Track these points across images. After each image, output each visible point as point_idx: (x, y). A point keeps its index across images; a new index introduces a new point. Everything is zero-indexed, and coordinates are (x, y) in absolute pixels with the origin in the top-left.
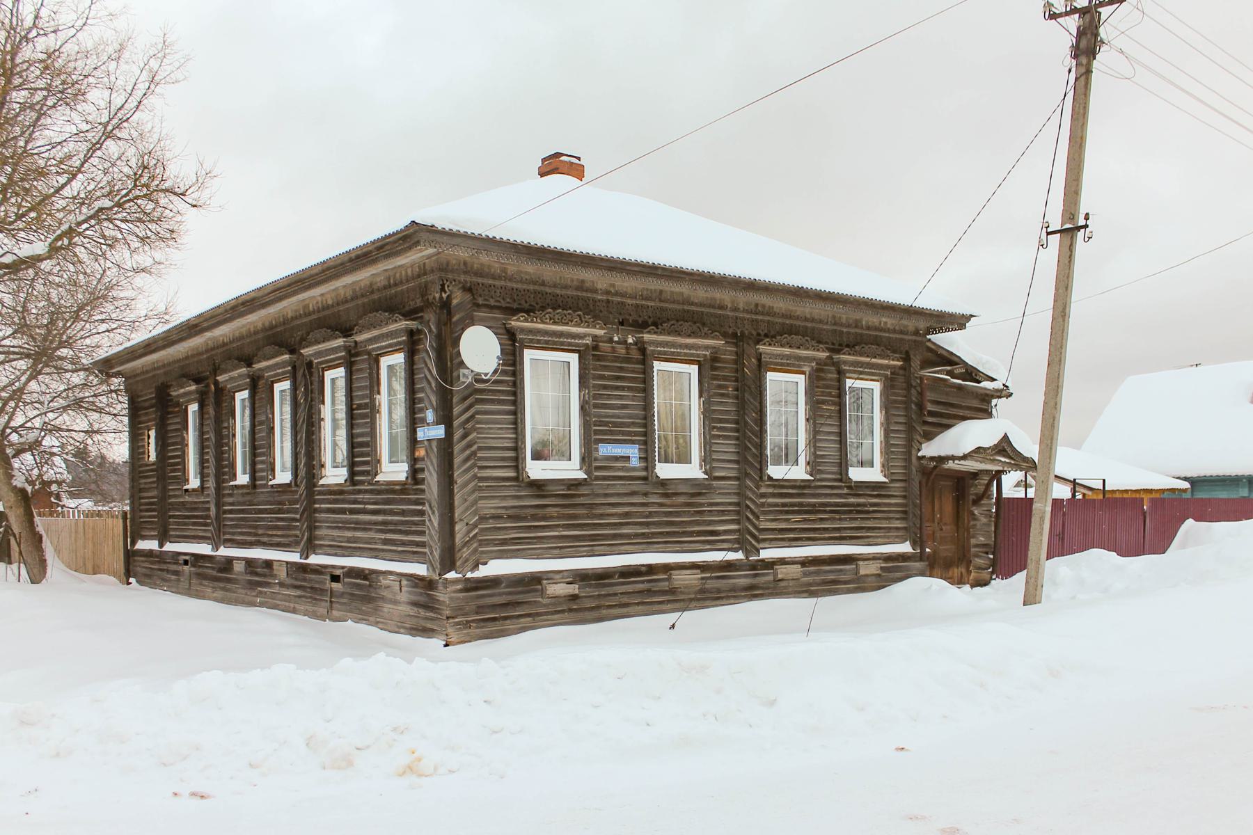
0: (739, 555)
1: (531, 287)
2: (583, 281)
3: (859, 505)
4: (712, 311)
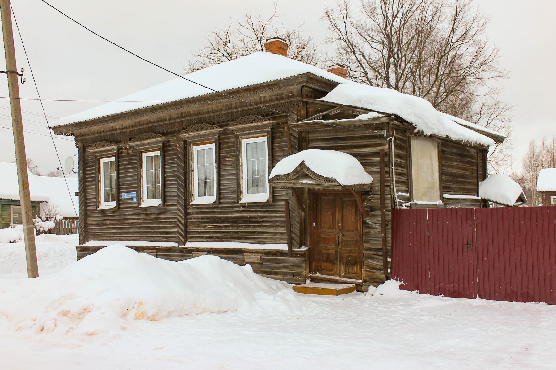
0: (175, 245)
2: (112, 127)
3: (250, 218)
4: (159, 124)
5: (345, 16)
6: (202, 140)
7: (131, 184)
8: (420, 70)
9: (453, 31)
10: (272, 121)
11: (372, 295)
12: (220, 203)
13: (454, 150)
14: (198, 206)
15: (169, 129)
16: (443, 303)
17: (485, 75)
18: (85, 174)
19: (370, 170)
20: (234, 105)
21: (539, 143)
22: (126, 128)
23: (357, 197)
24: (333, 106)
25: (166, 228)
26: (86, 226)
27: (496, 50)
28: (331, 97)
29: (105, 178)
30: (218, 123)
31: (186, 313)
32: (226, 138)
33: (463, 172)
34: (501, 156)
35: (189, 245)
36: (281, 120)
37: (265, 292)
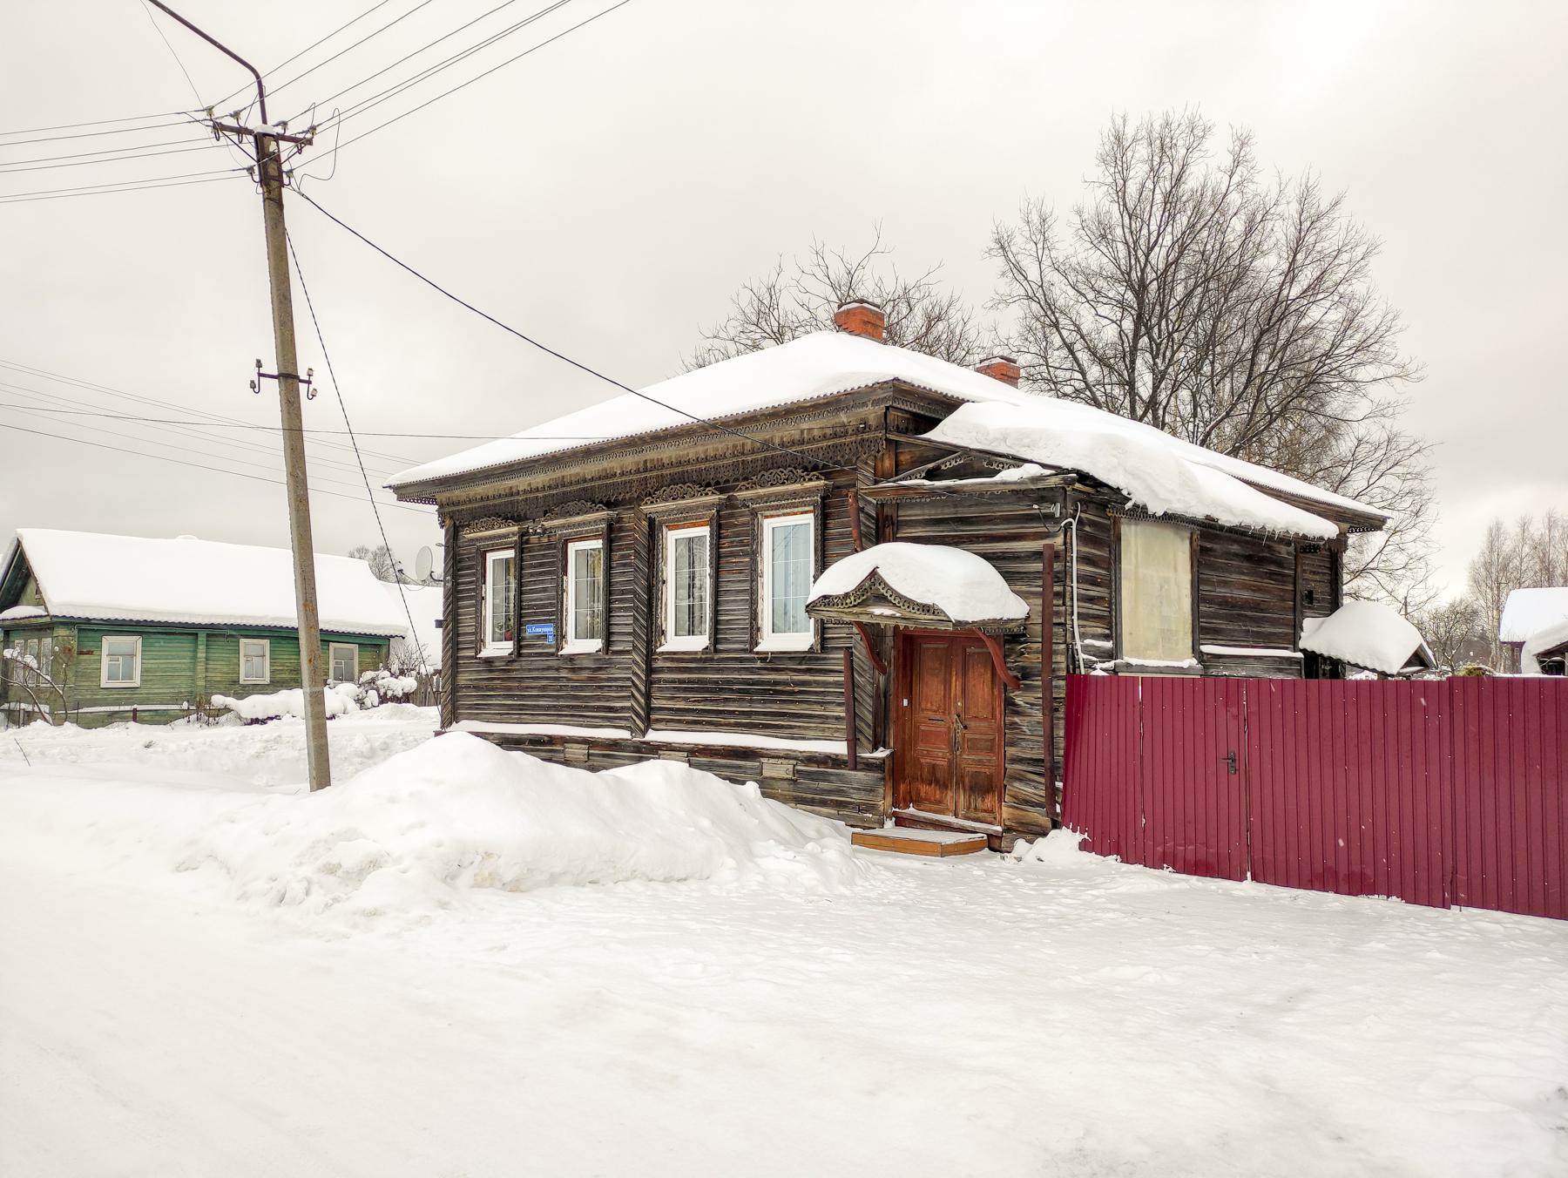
3: (776, 683)
5: (1040, 246)
6: (685, 519)
7: (544, 606)
8: (1212, 363)
9: (1291, 274)
10: (822, 482)
11: (1019, 859)
12: (716, 651)
13: (1235, 548)
14: (672, 656)
15: (620, 492)
16: (1165, 886)
17: (1362, 374)
18: (456, 584)
19: (1024, 588)
20: (748, 447)
21: (1511, 528)
22: (537, 490)
23: (991, 647)
24: (949, 450)
25: (608, 699)
26: (455, 689)
27: (1390, 317)
28: (946, 432)
29: (494, 594)
30: (718, 483)
31: (594, 878)
32: (732, 516)
33: (1258, 596)
34: (1400, 559)
35: (652, 736)
36: (842, 480)
37: (780, 841)
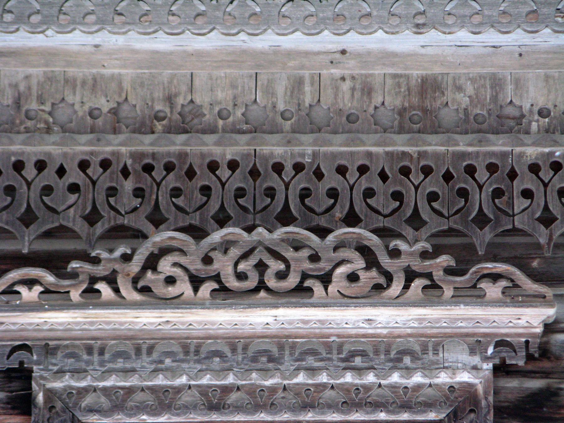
1: (120, 146)
2: (429, 86)
